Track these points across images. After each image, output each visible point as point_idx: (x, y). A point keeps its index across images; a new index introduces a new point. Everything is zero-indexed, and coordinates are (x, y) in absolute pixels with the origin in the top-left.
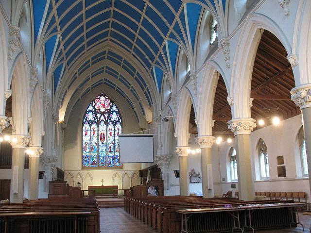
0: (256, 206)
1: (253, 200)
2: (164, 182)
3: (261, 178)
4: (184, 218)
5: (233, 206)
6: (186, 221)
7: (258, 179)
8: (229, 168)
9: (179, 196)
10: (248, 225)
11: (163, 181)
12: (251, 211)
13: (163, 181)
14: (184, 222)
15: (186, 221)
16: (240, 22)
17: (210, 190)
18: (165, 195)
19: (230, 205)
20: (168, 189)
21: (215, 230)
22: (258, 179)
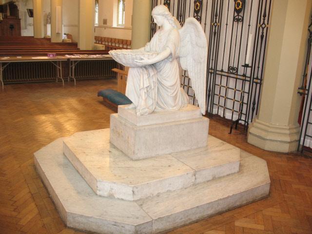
0: (95, 56)
1: (91, 49)
2: (21, 21)
3: (118, 25)
4: (72, 64)
5: (57, 55)
6: (73, 68)
7: (115, 25)
8: (116, 14)
9: (33, 37)
10: (72, 75)
11: (20, 19)
12: (75, 62)
13: (20, 19)
14: (72, 68)
15: (73, 68)
16: (208, 181)
17: (58, 33)
18: (22, 35)
19: (53, 55)
20: (26, 28)
21: (94, 76)
22: (115, 25)
